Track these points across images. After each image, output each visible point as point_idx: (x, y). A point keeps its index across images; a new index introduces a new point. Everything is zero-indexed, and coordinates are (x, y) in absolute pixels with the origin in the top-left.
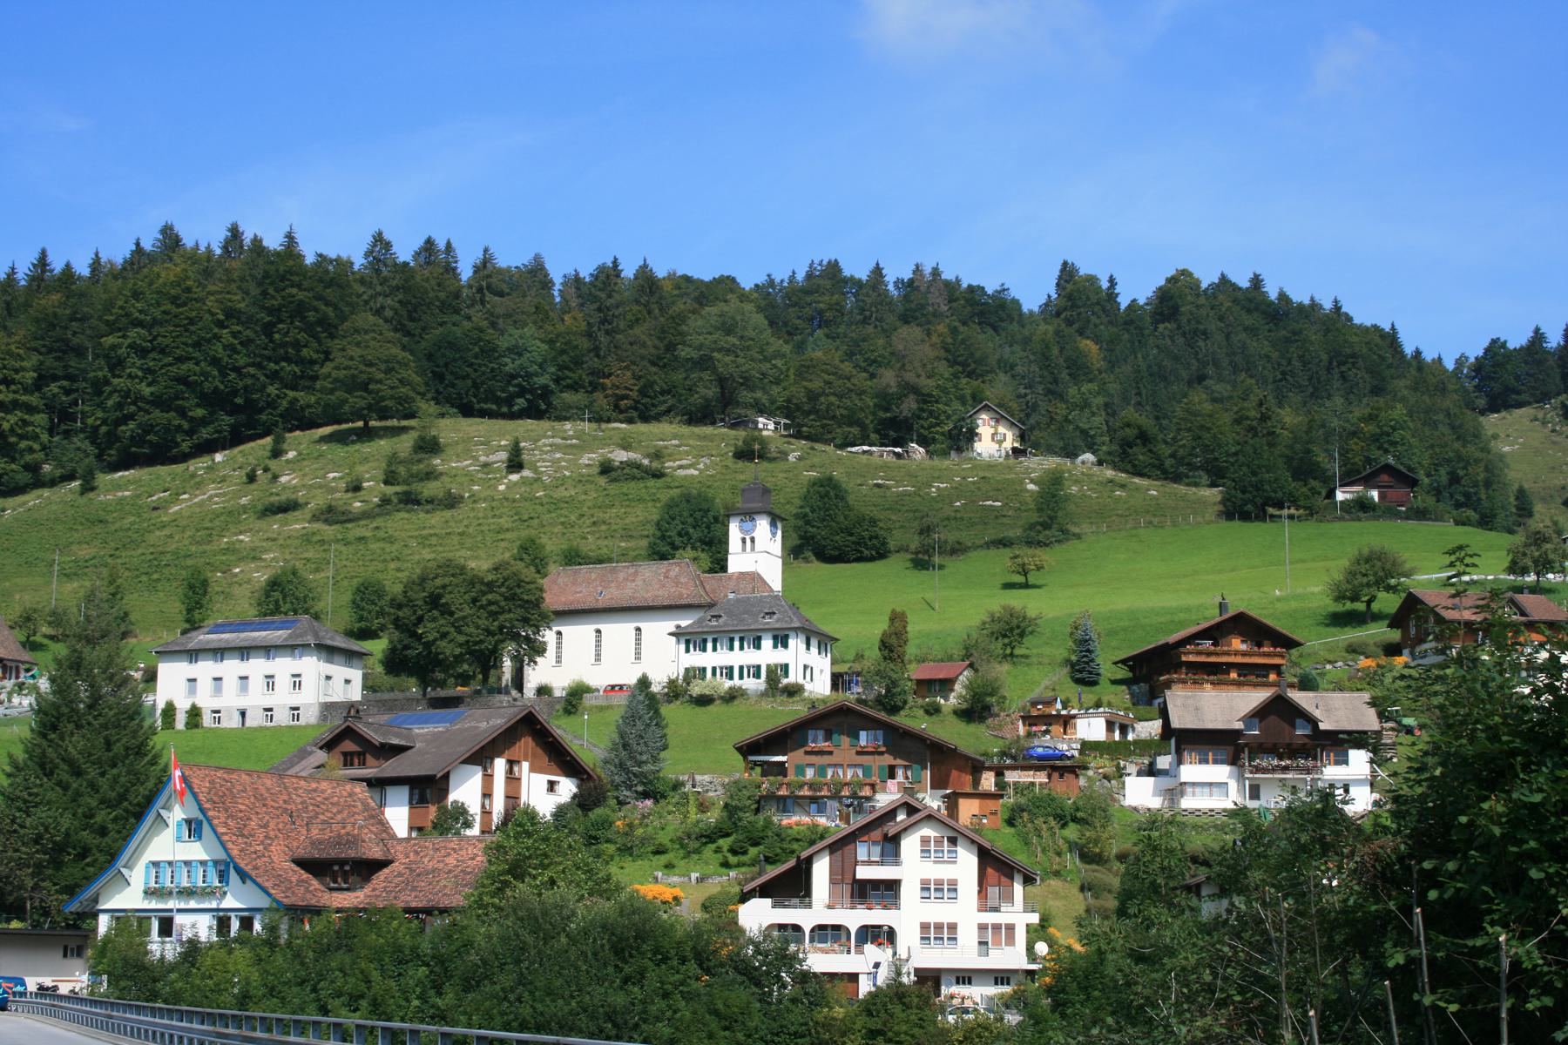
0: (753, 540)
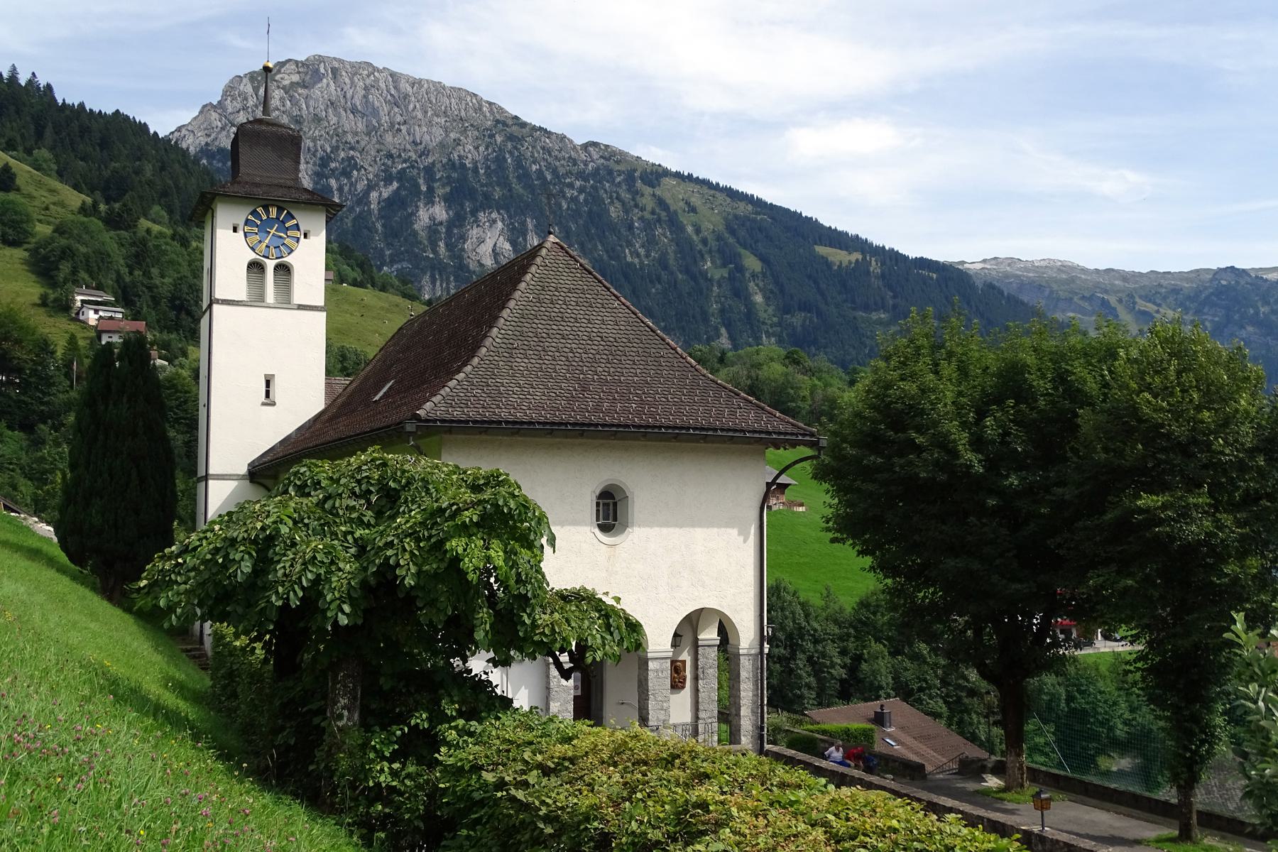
0: (284, 270)
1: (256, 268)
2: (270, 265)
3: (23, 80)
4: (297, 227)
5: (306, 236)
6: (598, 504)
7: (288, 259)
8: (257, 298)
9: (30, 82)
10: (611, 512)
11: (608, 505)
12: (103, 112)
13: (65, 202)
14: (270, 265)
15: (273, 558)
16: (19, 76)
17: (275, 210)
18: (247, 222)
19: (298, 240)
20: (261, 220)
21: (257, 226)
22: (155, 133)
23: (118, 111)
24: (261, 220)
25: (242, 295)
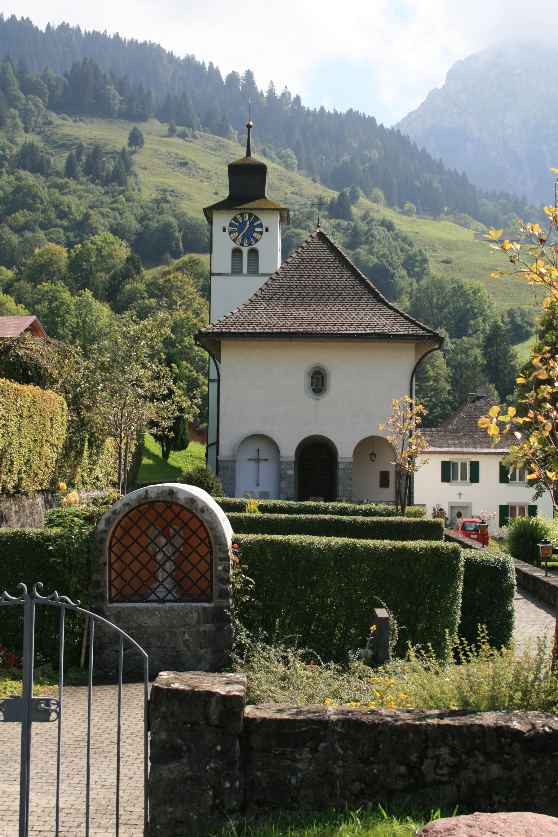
0: (254, 253)
1: (236, 253)
2: (245, 250)
3: (278, 92)
4: (261, 225)
5: (267, 230)
6: (312, 378)
7: (256, 246)
8: (236, 270)
9: (283, 95)
10: (320, 382)
11: (318, 378)
12: (339, 113)
13: (386, 218)
14: (245, 250)
15: (73, 248)
16: (275, 88)
17: (247, 216)
18: (231, 225)
19: (261, 233)
20: (239, 223)
21: (237, 227)
22: (382, 126)
23: (351, 110)
24: (239, 223)
25: (229, 270)
